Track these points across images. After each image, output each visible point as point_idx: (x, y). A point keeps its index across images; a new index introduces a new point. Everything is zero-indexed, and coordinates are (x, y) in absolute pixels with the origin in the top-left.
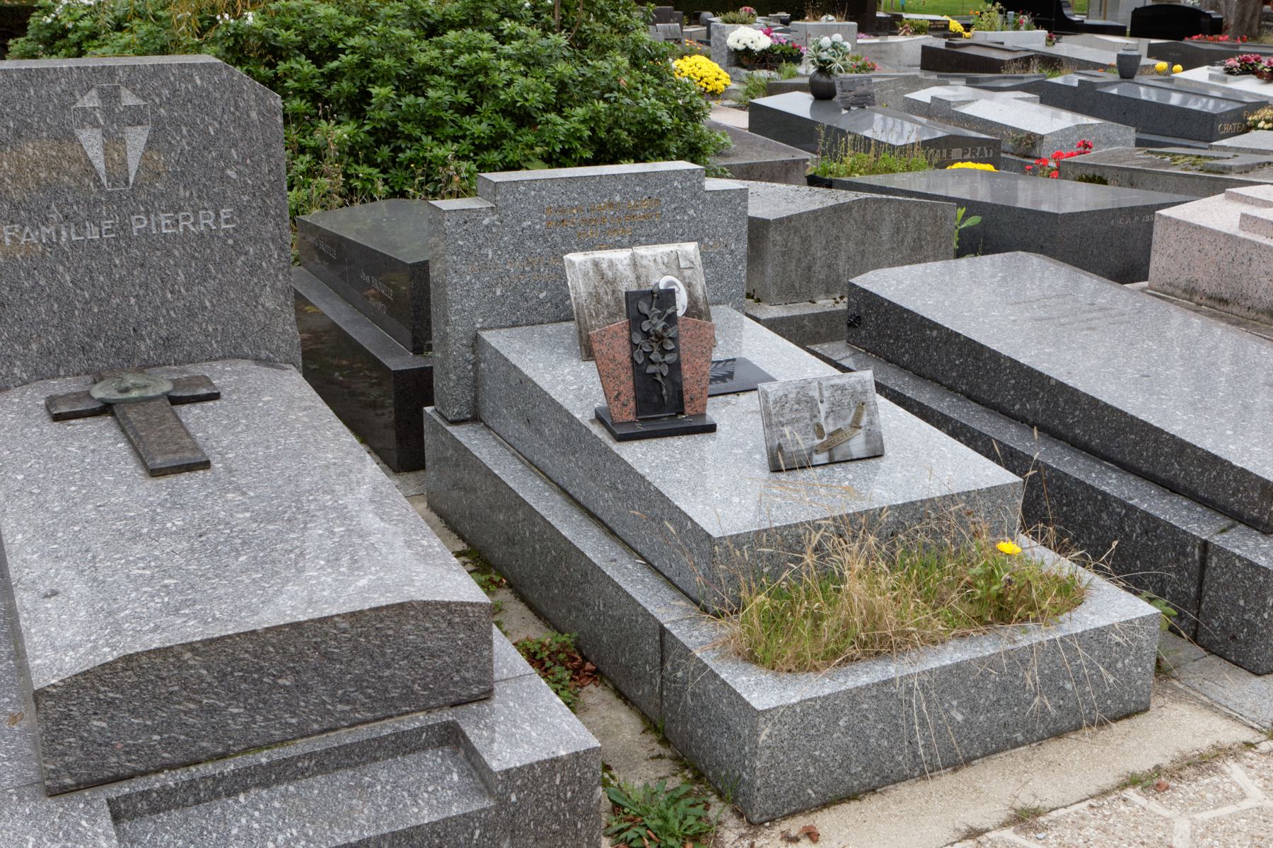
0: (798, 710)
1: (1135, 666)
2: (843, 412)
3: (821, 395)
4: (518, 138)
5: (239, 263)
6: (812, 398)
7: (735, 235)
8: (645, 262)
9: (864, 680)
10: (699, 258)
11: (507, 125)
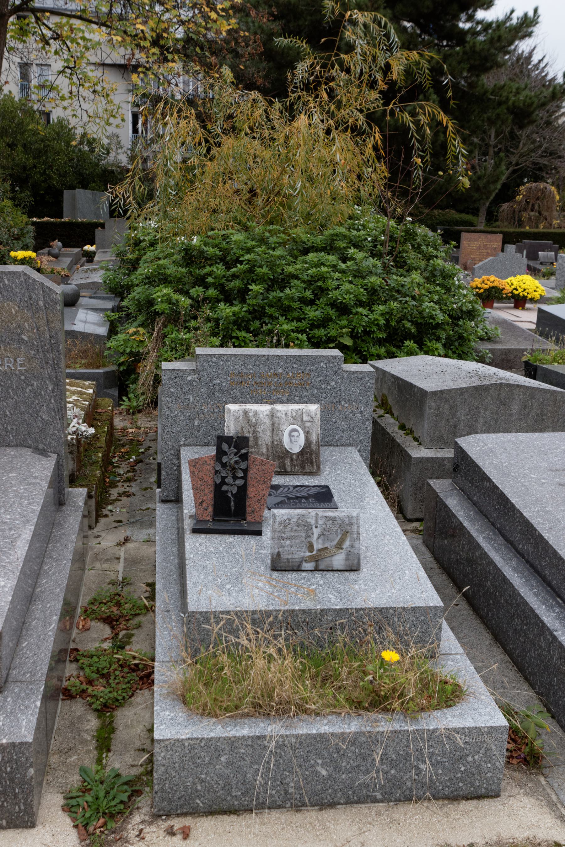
0: (187, 744)
1: (485, 762)
2: (331, 536)
3: (317, 522)
4: (338, 322)
5: (28, 390)
6: (309, 524)
7: (364, 401)
8: (279, 415)
9: (245, 732)
10: (319, 415)
11: (333, 313)
